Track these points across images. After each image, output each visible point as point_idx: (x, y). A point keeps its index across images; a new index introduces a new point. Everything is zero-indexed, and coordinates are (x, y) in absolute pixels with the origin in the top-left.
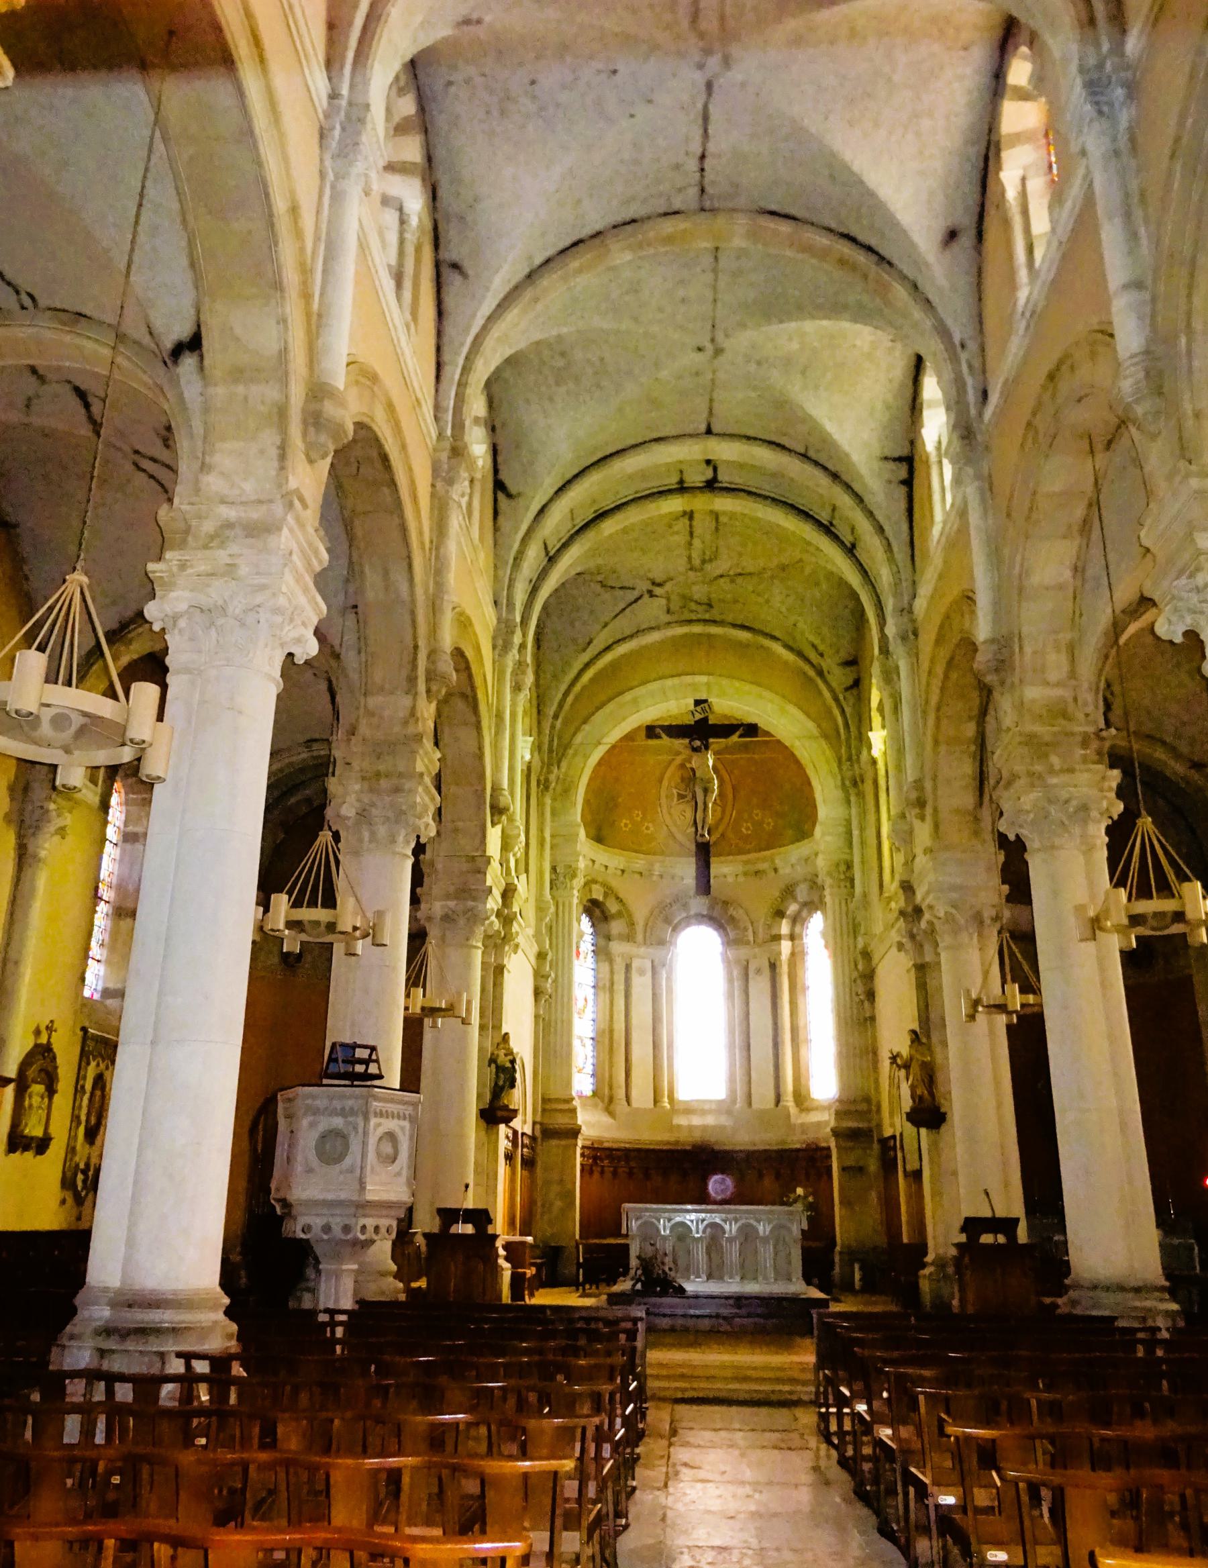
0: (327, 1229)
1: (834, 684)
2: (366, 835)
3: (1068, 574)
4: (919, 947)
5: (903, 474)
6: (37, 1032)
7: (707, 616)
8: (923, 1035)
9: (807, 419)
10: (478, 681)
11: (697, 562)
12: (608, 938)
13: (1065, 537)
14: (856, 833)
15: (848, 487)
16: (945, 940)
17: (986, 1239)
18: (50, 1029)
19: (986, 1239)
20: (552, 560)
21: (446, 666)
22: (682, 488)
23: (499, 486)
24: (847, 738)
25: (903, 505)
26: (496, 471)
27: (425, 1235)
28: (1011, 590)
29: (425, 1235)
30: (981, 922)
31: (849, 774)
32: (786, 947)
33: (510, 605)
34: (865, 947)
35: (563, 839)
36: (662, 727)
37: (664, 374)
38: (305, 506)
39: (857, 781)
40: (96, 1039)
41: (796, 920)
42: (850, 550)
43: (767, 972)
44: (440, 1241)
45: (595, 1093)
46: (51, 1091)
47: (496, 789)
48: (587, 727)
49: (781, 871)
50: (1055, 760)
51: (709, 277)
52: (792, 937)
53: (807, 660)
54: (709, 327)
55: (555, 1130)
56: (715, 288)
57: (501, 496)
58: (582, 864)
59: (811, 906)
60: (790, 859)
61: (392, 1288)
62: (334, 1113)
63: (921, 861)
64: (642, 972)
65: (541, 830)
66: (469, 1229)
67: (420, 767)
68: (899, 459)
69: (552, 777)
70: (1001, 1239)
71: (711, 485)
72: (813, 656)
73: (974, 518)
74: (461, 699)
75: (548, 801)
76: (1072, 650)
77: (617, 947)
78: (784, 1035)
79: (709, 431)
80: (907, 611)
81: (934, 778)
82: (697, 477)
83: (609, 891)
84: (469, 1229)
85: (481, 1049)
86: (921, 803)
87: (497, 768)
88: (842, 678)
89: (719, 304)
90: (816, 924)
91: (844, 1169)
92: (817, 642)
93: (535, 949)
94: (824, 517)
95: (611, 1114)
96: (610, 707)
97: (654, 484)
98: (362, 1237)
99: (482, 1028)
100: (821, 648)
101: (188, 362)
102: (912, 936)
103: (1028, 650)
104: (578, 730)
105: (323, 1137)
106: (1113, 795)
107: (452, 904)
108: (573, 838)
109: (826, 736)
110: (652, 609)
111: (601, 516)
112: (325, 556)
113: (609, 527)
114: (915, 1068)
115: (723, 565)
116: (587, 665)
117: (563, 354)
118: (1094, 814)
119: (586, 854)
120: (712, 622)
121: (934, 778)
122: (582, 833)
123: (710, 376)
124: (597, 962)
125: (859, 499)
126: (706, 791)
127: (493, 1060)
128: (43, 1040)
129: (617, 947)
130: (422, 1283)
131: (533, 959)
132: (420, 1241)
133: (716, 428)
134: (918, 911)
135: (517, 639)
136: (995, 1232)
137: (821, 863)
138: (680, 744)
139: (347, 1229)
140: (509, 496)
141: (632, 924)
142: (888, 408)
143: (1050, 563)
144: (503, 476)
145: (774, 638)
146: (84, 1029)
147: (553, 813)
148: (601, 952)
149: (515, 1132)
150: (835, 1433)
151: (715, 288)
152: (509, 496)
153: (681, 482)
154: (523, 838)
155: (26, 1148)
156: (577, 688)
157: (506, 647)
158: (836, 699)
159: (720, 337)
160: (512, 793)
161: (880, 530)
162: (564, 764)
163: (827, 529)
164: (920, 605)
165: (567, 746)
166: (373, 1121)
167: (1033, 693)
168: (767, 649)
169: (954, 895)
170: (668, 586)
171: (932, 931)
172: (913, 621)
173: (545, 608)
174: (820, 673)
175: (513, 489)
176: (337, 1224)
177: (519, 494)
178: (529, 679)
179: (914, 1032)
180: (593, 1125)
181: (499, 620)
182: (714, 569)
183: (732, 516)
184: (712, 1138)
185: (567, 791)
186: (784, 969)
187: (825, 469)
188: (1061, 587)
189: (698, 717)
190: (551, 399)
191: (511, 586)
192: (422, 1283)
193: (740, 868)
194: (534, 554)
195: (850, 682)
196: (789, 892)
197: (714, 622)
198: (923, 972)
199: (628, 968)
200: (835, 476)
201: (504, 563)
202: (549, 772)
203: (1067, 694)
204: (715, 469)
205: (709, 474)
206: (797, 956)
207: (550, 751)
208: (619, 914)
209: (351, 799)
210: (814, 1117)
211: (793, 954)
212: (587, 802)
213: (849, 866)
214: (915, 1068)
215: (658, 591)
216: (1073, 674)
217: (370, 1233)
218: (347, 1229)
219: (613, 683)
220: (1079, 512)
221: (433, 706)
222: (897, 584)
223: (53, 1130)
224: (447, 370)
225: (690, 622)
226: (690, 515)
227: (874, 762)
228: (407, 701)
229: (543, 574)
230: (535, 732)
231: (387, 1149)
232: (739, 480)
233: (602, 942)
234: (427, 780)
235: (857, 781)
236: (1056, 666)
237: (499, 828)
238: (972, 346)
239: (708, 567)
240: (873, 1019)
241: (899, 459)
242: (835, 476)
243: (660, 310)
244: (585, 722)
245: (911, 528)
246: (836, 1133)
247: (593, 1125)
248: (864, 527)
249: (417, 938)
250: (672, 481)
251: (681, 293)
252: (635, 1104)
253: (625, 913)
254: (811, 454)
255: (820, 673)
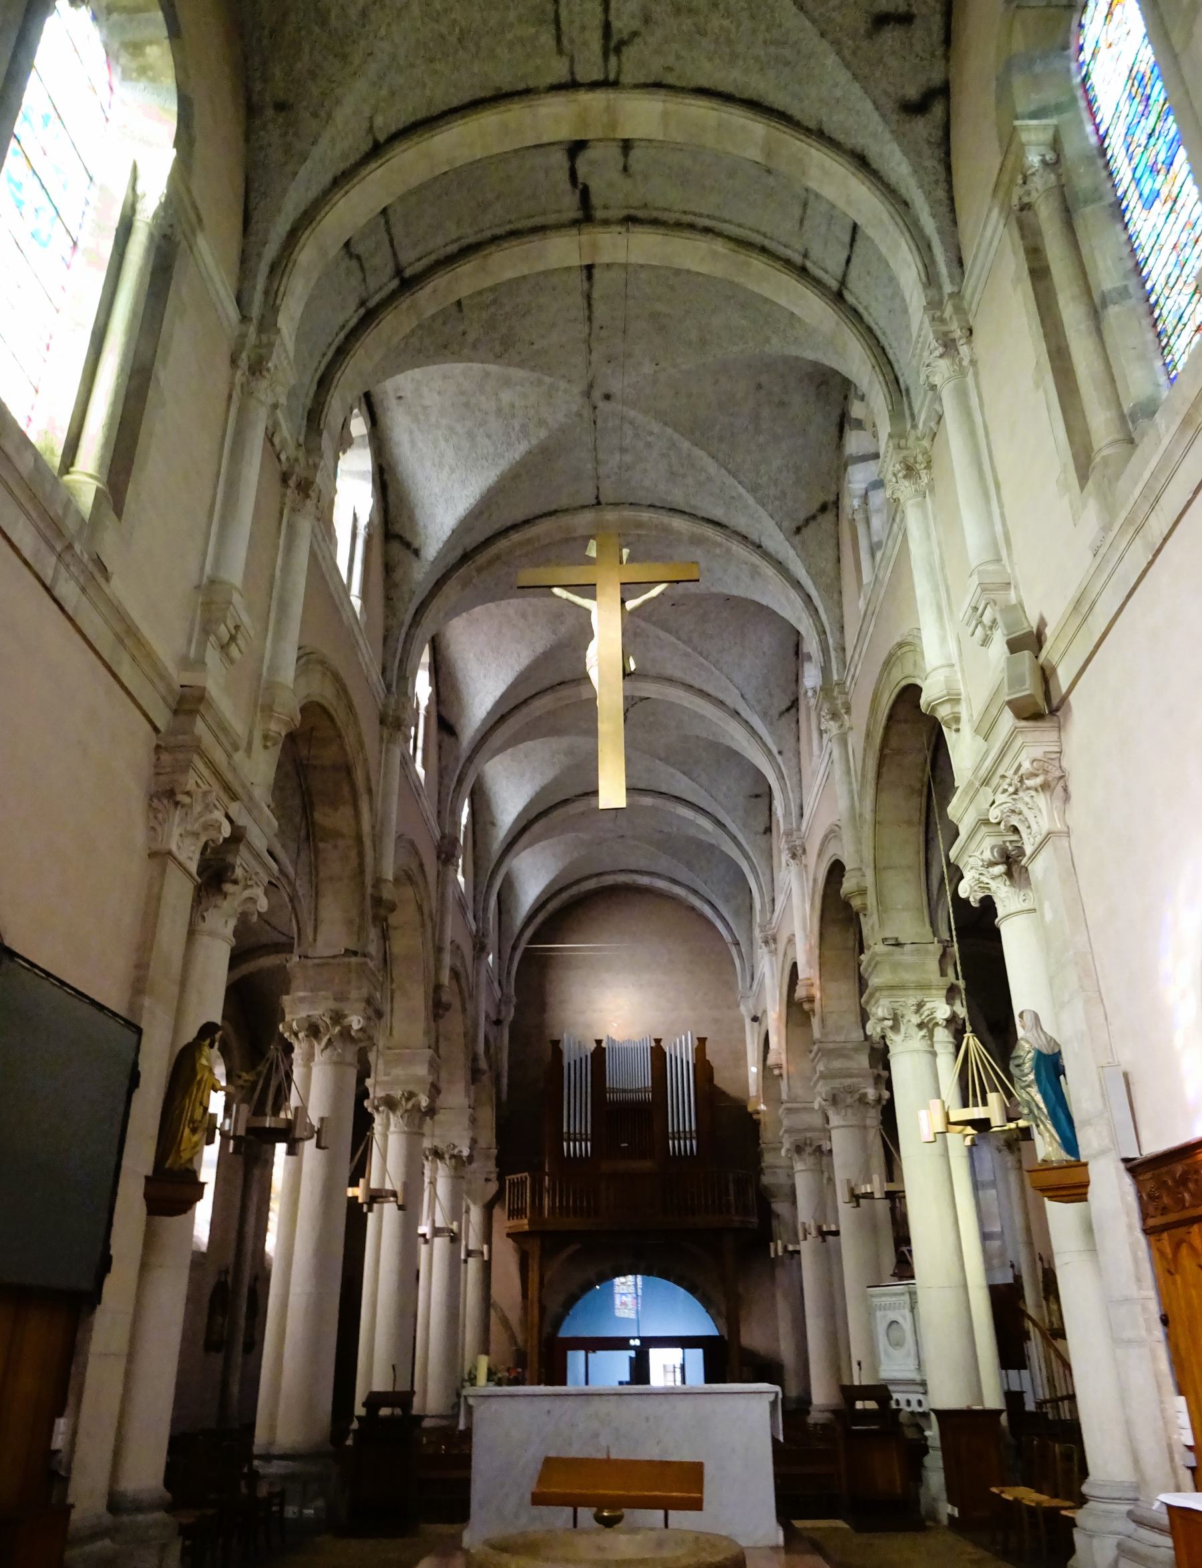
0: (909, 1403)
17: (384, 1411)
19: (384, 1411)
51: (603, 471)
54: (599, 423)
56: (597, 461)
66: (871, 1405)
70: (398, 1411)
73: (317, 530)
84: (871, 1405)
89: (591, 446)
98: (920, 1410)
117: (759, 387)
123: (595, 357)
151: (597, 461)
159: (587, 413)
176: (914, 1398)
223: (416, 1389)
243: (649, 445)
251: (628, 458)
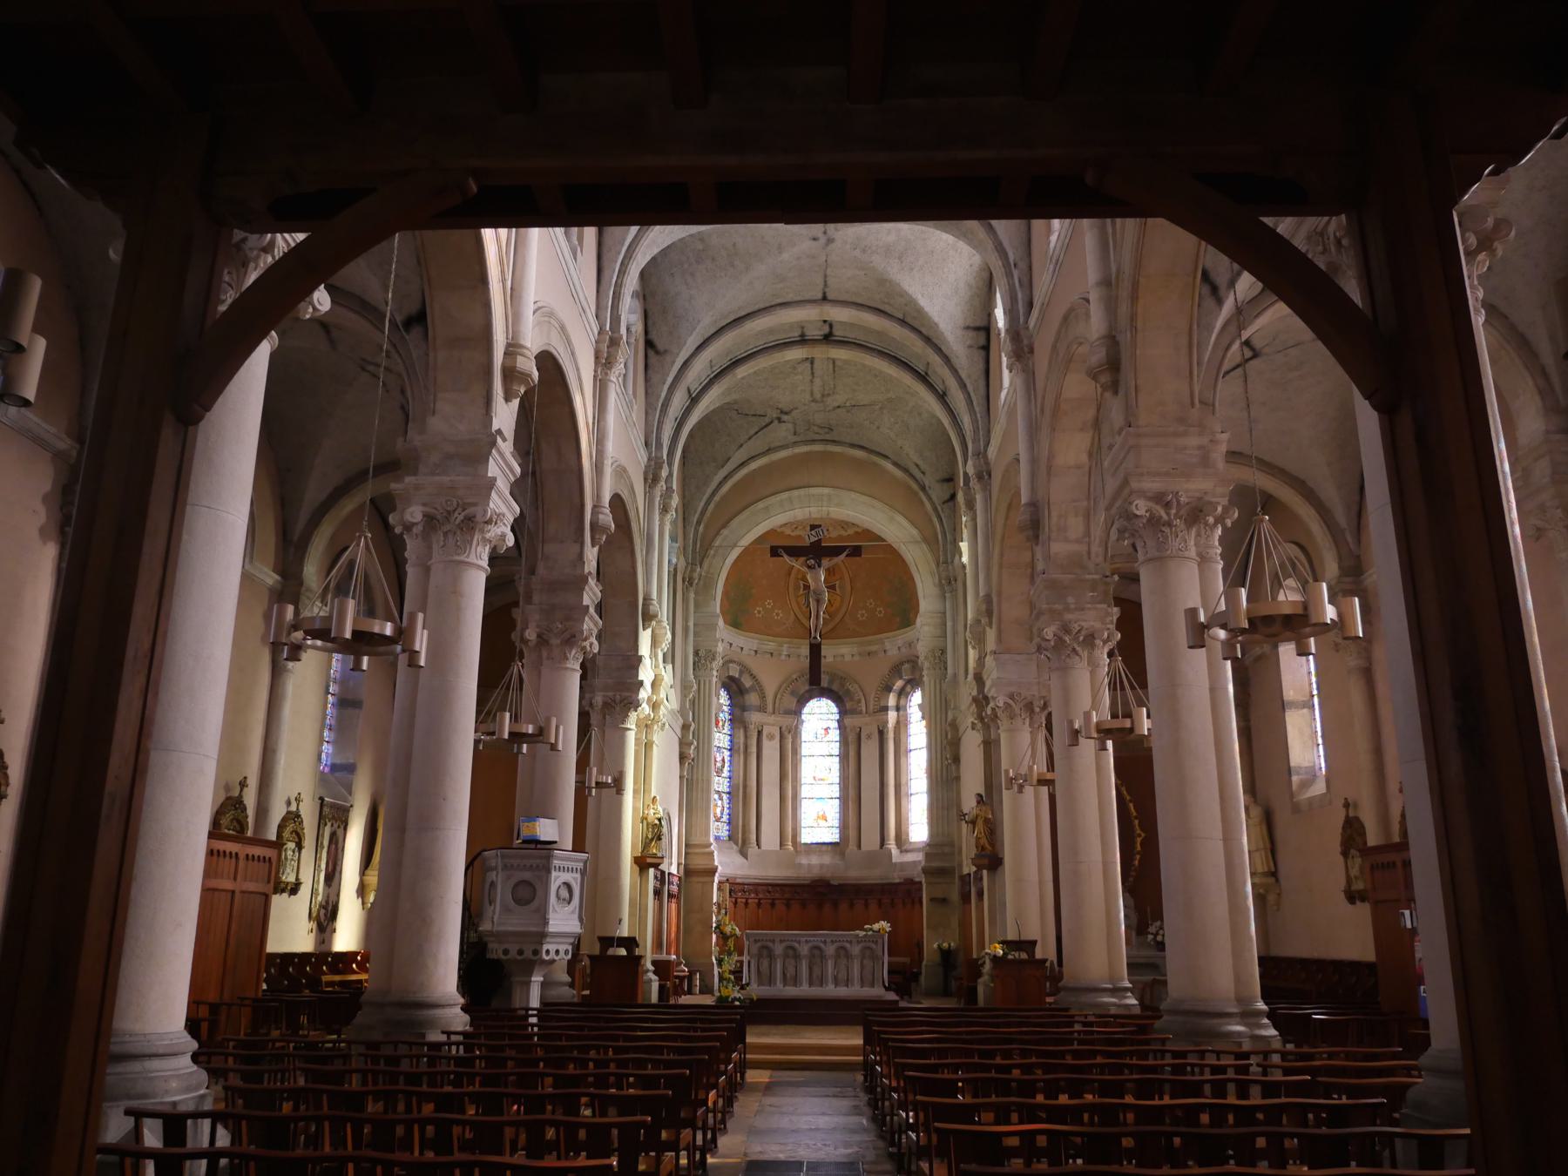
1: (934, 498)
2: (545, 654)
3: (1084, 458)
4: (986, 727)
5: (982, 342)
6: (289, 803)
7: (828, 437)
8: (989, 798)
9: (903, 294)
10: (632, 514)
11: (818, 396)
12: (744, 709)
13: (1082, 430)
14: (949, 624)
15: (938, 350)
16: (1004, 724)
18: (298, 800)
20: (694, 400)
21: (607, 518)
22: (803, 341)
23: (649, 344)
24: (944, 551)
25: (981, 366)
26: (646, 332)
27: (591, 957)
28: (1043, 468)
29: (591, 957)
30: (1032, 711)
31: (944, 574)
32: (892, 716)
33: (659, 445)
34: (954, 720)
35: (704, 628)
36: (784, 548)
37: (785, 256)
38: (504, 440)
39: (950, 581)
40: (333, 806)
41: (903, 694)
42: (942, 397)
43: (876, 736)
44: (600, 961)
45: (730, 838)
46: (300, 846)
47: (647, 599)
48: (725, 532)
49: (889, 653)
50: (1070, 600)
52: (898, 709)
53: (912, 476)
55: (697, 873)
57: (651, 353)
58: (720, 648)
59: (914, 683)
60: (893, 645)
61: (566, 994)
62: (525, 868)
63: (989, 660)
64: (771, 737)
65: (686, 619)
66: (623, 952)
67: (586, 601)
68: (977, 329)
69: (696, 575)
70: (1024, 956)
71: (828, 338)
72: (918, 475)
74: (620, 539)
75: (692, 595)
76: (1087, 517)
77: (754, 718)
78: (888, 790)
79: (825, 298)
80: (981, 454)
81: (999, 594)
82: (815, 332)
83: (745, 669)
84: (623, 952)
85: (635, 809)
86: (989, 613)
87: (648, 581)
88: (940, 492)
90: (917, 698)
91: (932, 900)
92: (920, 463)
93: (681, 721)
94: (921, 368)
95: (744, 854)
96: (746, 513)
97: (781, 337)
99: (636, 792)
100: (923, 466)
101: (416, 331)
102: (981, 719)
103: (1054, 514)
104: (718, 533)
105: (517, 885)
106: (1112, 627)
107: (610, 694)
108: (714, 627)
109: (925, 540)
110: (782, 432)
111: (736, 363)
112: (518, 470)
113: (742, 372)
114: (980, 822)
115: (839, 399)
116: (726, 479)
118: (1098, 642)
119: (725, 639)
120: (834, 448)
121: (999, 594)
122: (721, 622)
124: (732, 729)
125: (947, 360)
126: (818, 601)
127: (644, 819)
128: (293, 808)
129: (754, 718)
130: (587, 992)
131: (679, 731)
132: (586, 962)
133: (830, 296)
134: (986, 698)
135: (664, 473)
136: (1019, 950)
137: (922, 649)
138: (797, 564)
139: (521, 952)
140: (657, 352)
141: (763, 697)
142: (970, 286)
143: (1072, 449)
144: (653, 336)
145: (886, 457)
146: (322, 799)
147: (697, 606)
148: (737, 720)
149: (663, 873)
150: (1028, 1164)
152: (657, 352)
153: (802, 335)
154: (669, 636)
155: (283, 891)
156: (717, 498)
157: (656, 479)
158: (935, 509)
160: (660, 603)
161: (963, 386)
162: (706, 565)
163: (923, 378)
164: (992, 452)
165: (710, 546)
166: (554, 874)
167: (1057, 548)
168: (875, 464)
169: (1013, 689)
170: (794, 413)
171: (995, 716)
172: (987, 463)
173: (691, 435)
174: (923, 488)
175: (660, 346)
177: (666, 351)
178: (675, 501)
179: (980, 795)
180: (727, 864)
181: (649, 459)
182: (832, 402)
183: (846, 362)
184: (827, 874)
185: (709, 583)
186: (891, 735)
187: (919, 332)
188: (1078, 467)
189: (813, 539)
190: (692, 275)
191: (660, 423)
192: (587, 992)
193: (855, 650)
194: (679, 401)
195: (947, 496)
196: (896, 671)
197: (834, 442)
198: (990, 747)
199: (760, 733)
200: (928, 340)
201: (654, 407)
202: (693, 571)
203: (1084, 548)
204: (831, 326)
205: (826, 329)
206: (902, 724)
207: (694, 551)
208: (752, 688)
209: (532, 625)
210: (910, 857)
211: (898, 722)
212: (725, 593)
213: (943, 652)
214: (980, 822)
215: (785, 418)
216: (1088, 533)
217: (552, 955)
218: (521, 952)
219: (751, 492)
220: (1091, 413)
221: (596, 549)
222: (976, 430)
223: (302, 878)
224: (606, 273)
225: (813, 441)
226: (812, 361)
227: (964, 566)
228: (577, 547)
229: (687, 412)
230: (680, 539)
231: (564, 893)
232: (851, 335)
233: (737, 712)
234: (592, 610)
235: (950, 581)
236: (1075, 526)
237: (649, 631)
238: (1023, 265)
239: (829, 400)
240: (958, 778)
241: (977, 329)
242: (928, 340)
244: (724, 526)
245: (988, 385)
246: (925, 871)
247: (727, 864)
248: (952, 383)
249: (584, 716)
250: (796, 334)
252: (764, 847)
253: (759, 687)
254: (908, 320)
255: (923, 488)
